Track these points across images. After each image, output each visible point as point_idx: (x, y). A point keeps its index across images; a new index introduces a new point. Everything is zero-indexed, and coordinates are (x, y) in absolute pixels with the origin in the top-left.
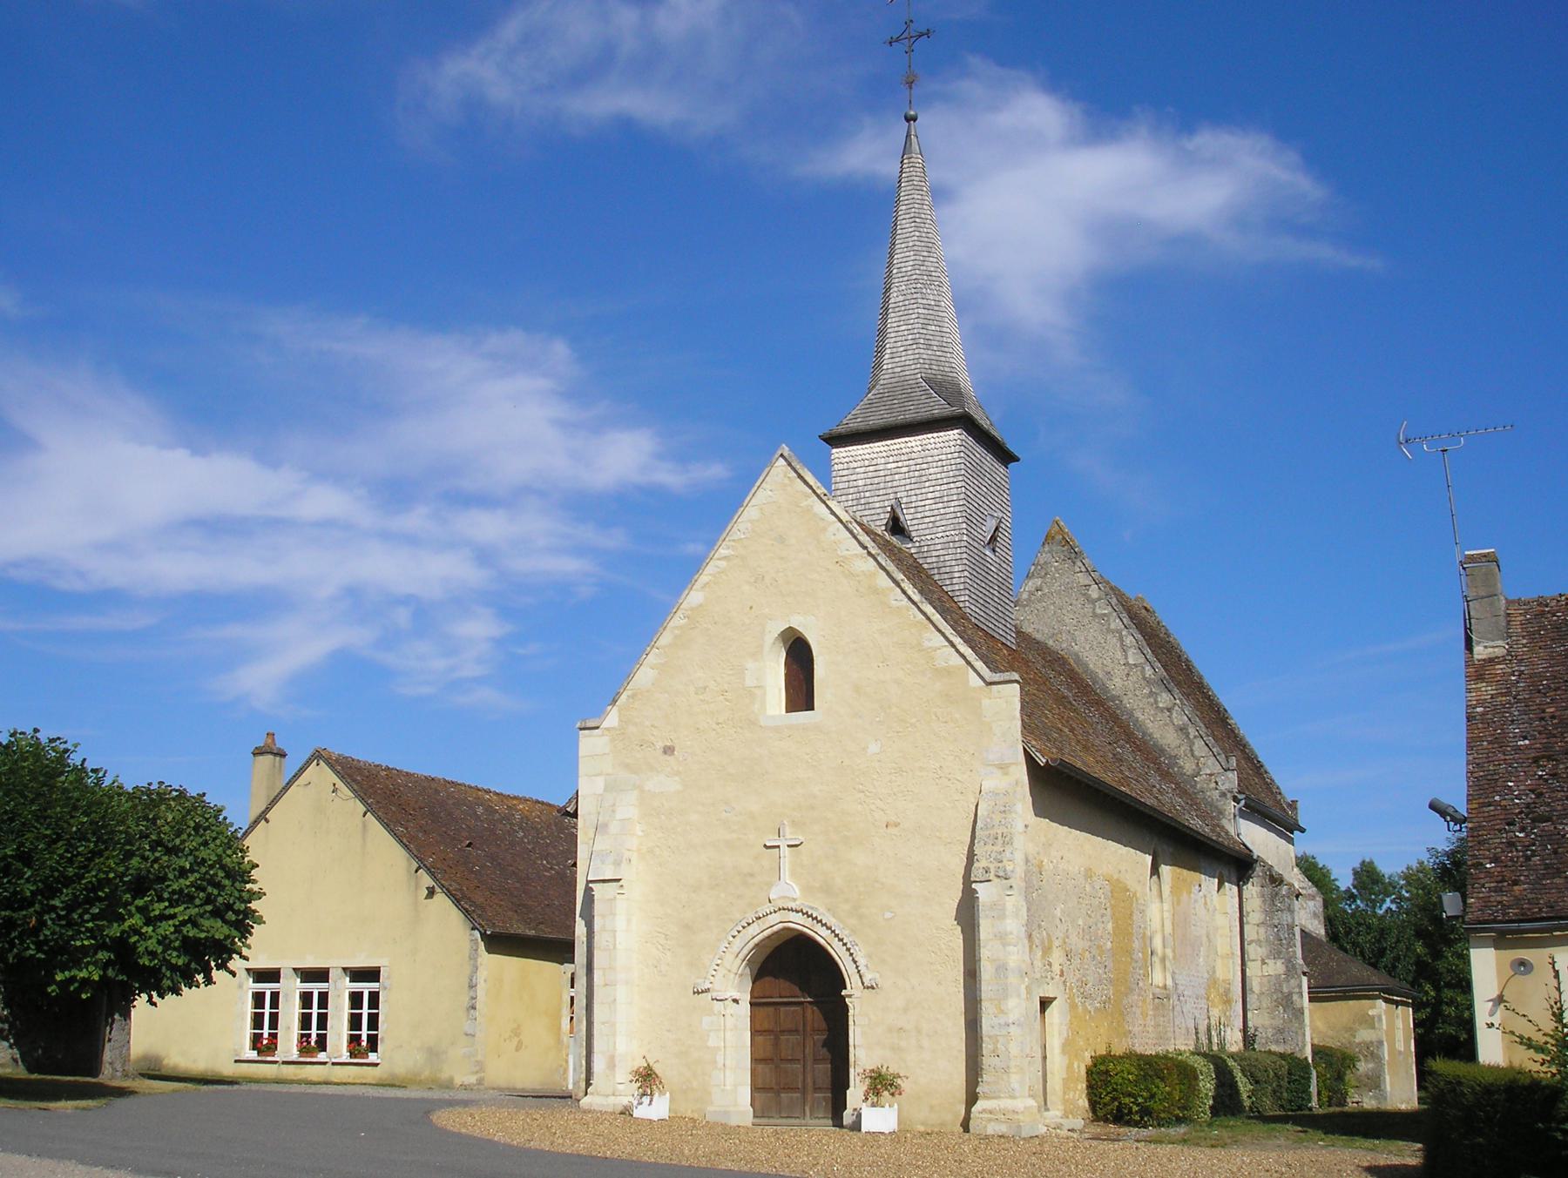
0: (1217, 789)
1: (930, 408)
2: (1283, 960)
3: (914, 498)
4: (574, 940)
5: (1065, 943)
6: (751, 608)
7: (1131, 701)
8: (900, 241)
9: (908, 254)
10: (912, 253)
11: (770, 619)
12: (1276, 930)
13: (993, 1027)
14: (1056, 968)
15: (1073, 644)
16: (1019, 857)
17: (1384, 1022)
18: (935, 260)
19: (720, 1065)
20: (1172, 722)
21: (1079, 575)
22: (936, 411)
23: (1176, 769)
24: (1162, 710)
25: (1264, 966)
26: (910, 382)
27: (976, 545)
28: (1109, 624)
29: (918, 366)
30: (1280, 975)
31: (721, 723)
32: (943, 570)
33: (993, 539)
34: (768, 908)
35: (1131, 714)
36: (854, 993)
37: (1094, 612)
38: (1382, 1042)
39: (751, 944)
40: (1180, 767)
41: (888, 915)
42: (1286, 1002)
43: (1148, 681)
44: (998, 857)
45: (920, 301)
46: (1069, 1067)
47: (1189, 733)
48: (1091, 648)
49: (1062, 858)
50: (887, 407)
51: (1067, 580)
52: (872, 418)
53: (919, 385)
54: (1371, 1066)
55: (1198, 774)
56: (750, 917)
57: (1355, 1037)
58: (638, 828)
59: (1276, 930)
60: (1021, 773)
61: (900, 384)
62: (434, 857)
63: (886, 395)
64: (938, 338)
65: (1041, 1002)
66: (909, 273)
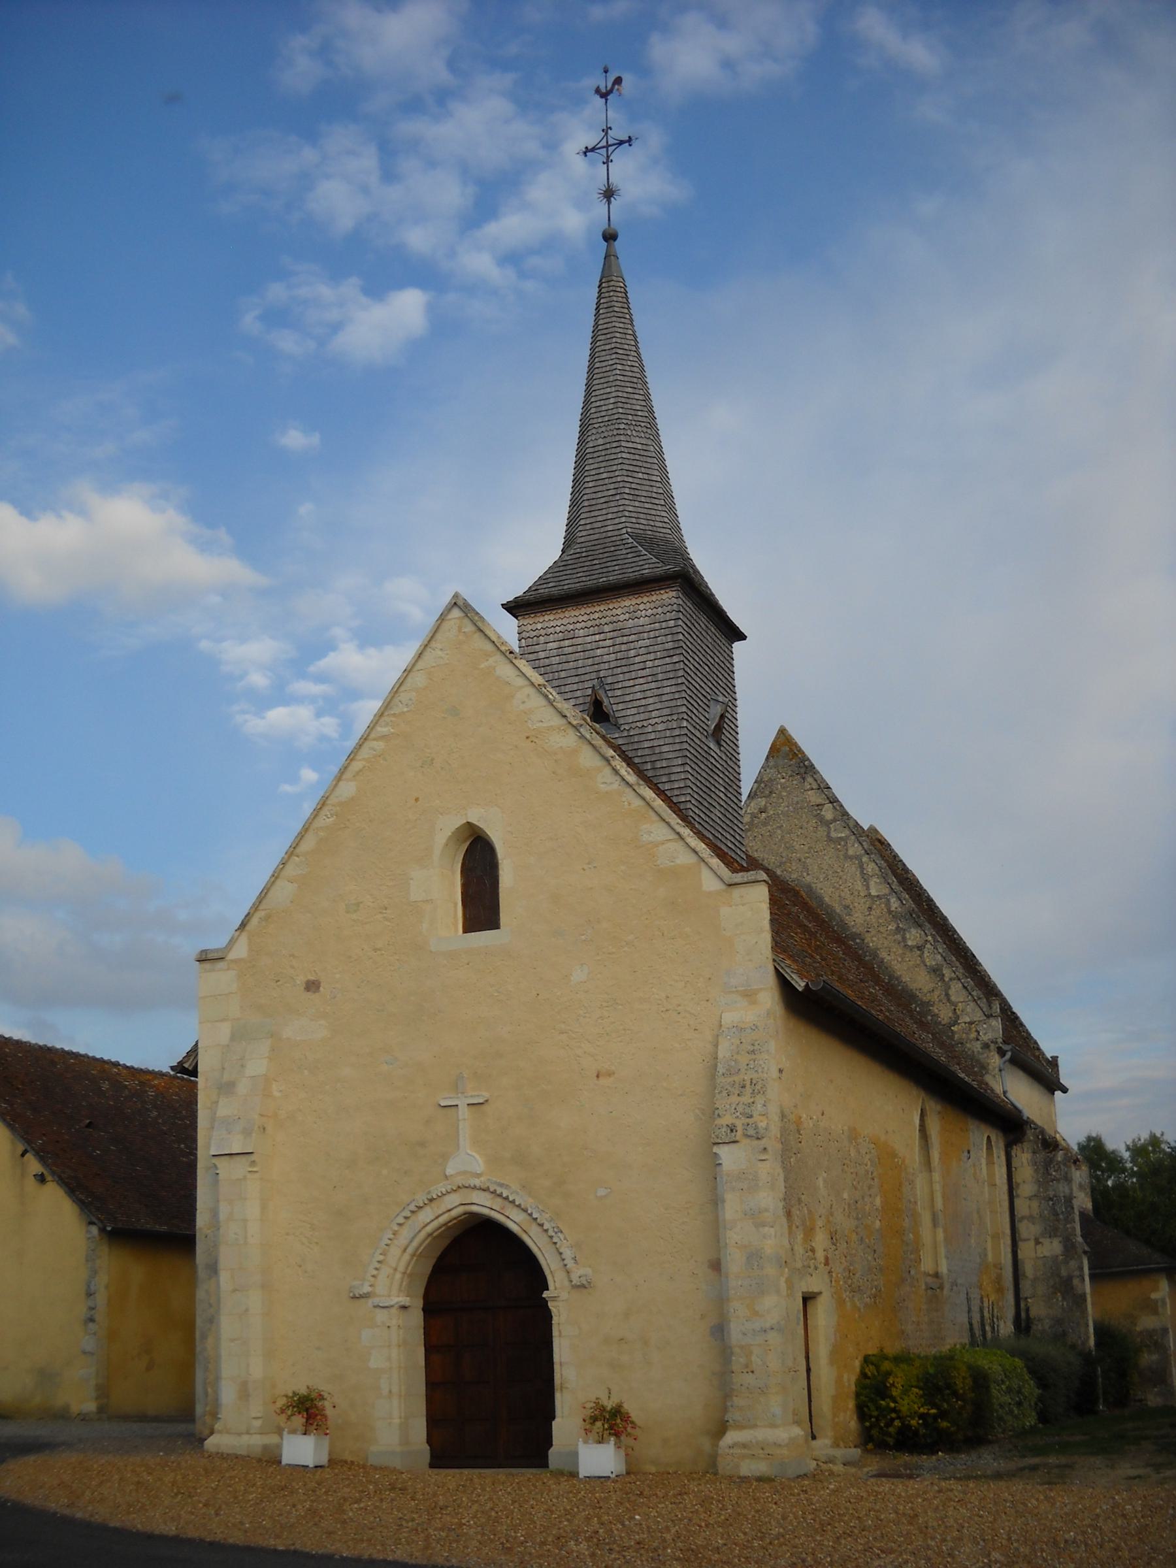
0: (978, 1040)
1: (638, 568)
2: (1061, 1239)
3: (621, 677)
4: (195, 1235)
5: (829, 1221)
6: (417, 800)
7: (874, 939)
8: (599, 376)
9: (608, 390)
10: (613, 389)
11: (441, 814)
12: (1051, 1203)
13: (745, 1334)
14: (820, 1255)
15: (805, 874)
16: (773, 1110)
17: (1168, 1306)
18: (641, 397)
19: (385, 1392)
20: (923, 962)
21: (809, 792)
22: (647, 571)
23: (929, 1018)
24: (911, 948)
25: (1038, 1247)
26: (614, 539)
27: (698, 734)
28: (847, 850)
29: (623, 519)
30: (1057, 1256)
31: (380, 950)
32: (658, 765)
33: (719, 728)
34: (442, 1188)
35: (875, 954)
36: (558, 1294)
37: (828, 836)
38: (1168, 1329)
39: (423, 1234)
40: (934, 1015)
41: (601, 1192)
42: (1065, 1287)
43: (895, 916)
44: (746, 1111)
45: (623, 444)
46: (839, 1380)
47: (943, 975)
48: (827, 878)
49: (823, 1114)
50: (585, 569)
51: (795, 799)
52: (566, 582)
53: (624, 542)
54: (1155, 1357)
55: (955, 1023)
56: (421, 1198)
57: (1136, 1325)
58: (274, 1086)
59: (1051, 1203)
60: (769, 999)
61: (601, 541)
62: (44, 1138)
63: (584, 554)
64: (647, 488)
65: (803, 1298)
66: (610, 412)
